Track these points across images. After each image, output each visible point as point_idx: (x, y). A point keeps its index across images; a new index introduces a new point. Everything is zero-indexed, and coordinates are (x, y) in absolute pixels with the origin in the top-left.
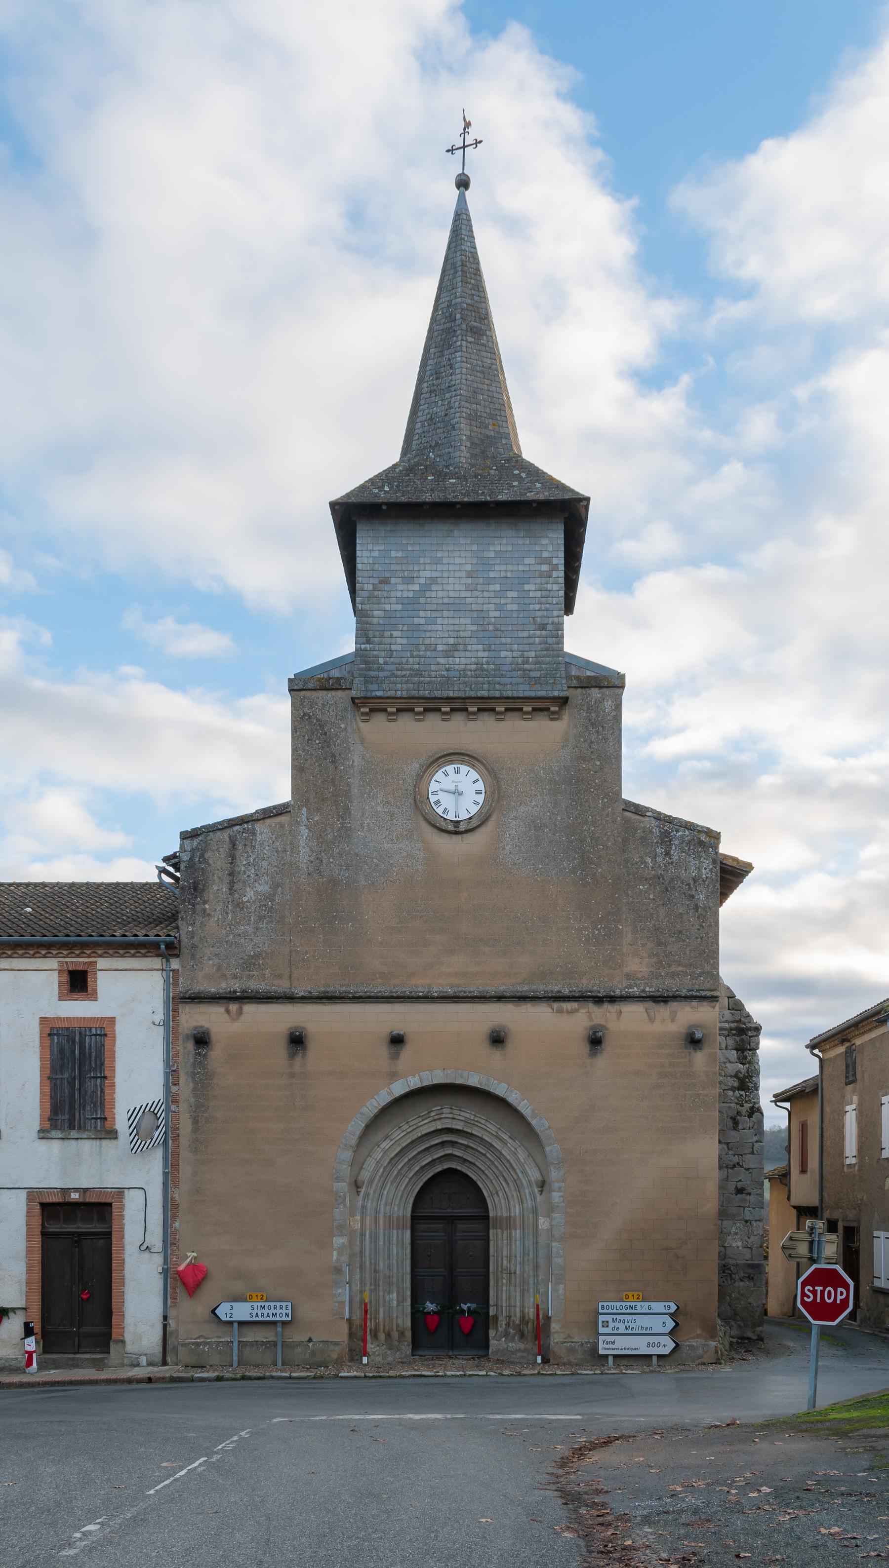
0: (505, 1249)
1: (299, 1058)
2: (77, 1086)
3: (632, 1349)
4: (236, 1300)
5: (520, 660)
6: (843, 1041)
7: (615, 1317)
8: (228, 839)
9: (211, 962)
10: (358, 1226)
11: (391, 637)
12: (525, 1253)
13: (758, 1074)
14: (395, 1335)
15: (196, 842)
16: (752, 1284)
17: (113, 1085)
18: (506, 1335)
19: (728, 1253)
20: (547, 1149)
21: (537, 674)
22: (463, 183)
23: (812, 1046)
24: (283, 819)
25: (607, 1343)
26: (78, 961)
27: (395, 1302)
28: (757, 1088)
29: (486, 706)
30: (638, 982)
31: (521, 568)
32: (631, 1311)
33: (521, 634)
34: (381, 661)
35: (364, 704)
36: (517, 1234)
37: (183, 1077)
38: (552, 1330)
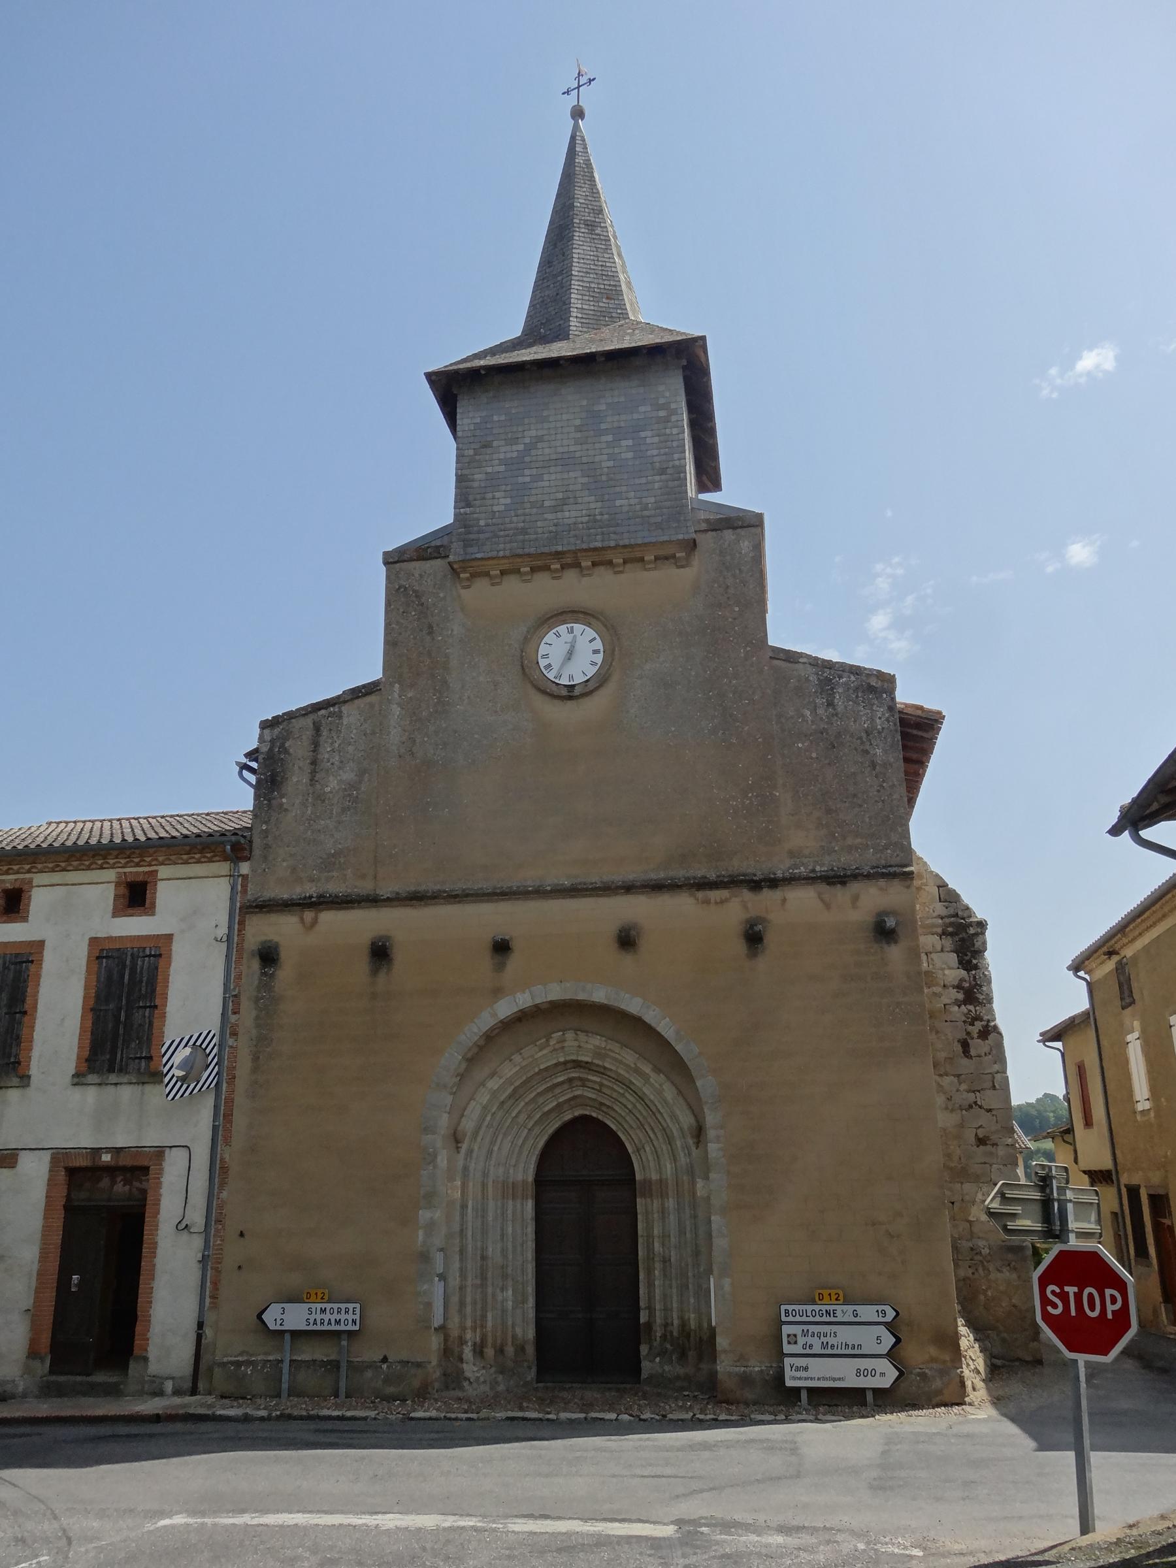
0: (658, 1226)
1: (382, 977)
2: (123, 1018)
3: (834, 1379)
4: (290, 1300)
5: (638, 507)
6: (1110, 954)
7: (805, 1327)
8: (311, 725)
9: (285, 864)
10: (458, 1195)
11: (493, 498)
12: (682, 1232)
13: (989, 982)
14: (510, 1350)
15: (277, 731)
16: (1014, 1276)
17: (163, 1015)
18: (663, 1353)
19: (975, 1229)
20: (699, 1083)
21: (659, 519)
22: (578, 113)
23: (1076, 967)
24: (372, 698)
25: (798, 1369)
26: (134, 871)
27: (510, 1303)
28: (990, 1000)
29: (601, 559)
30: (805, 860)
31: (635, 416)
32: (828, 1319)
33: (637, 481)
34: (482, 523)
35: (464, 570)
36: (671, 1203)
37: (246, 1005)
38: (718, 1348)
